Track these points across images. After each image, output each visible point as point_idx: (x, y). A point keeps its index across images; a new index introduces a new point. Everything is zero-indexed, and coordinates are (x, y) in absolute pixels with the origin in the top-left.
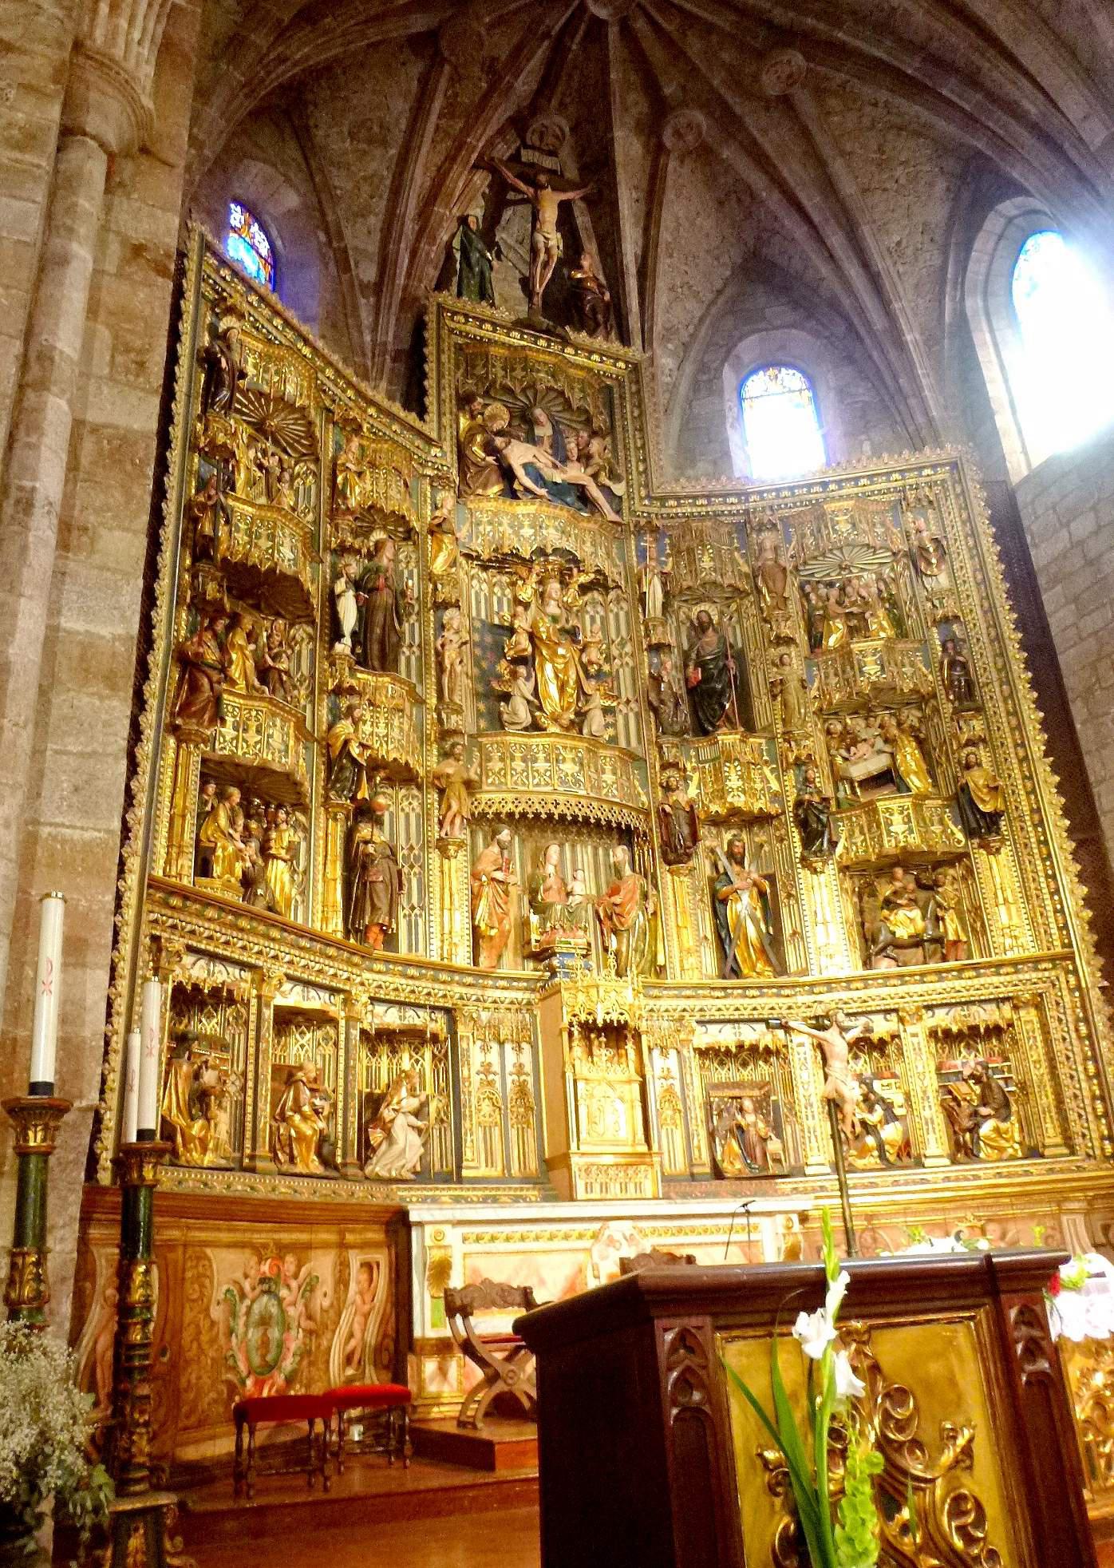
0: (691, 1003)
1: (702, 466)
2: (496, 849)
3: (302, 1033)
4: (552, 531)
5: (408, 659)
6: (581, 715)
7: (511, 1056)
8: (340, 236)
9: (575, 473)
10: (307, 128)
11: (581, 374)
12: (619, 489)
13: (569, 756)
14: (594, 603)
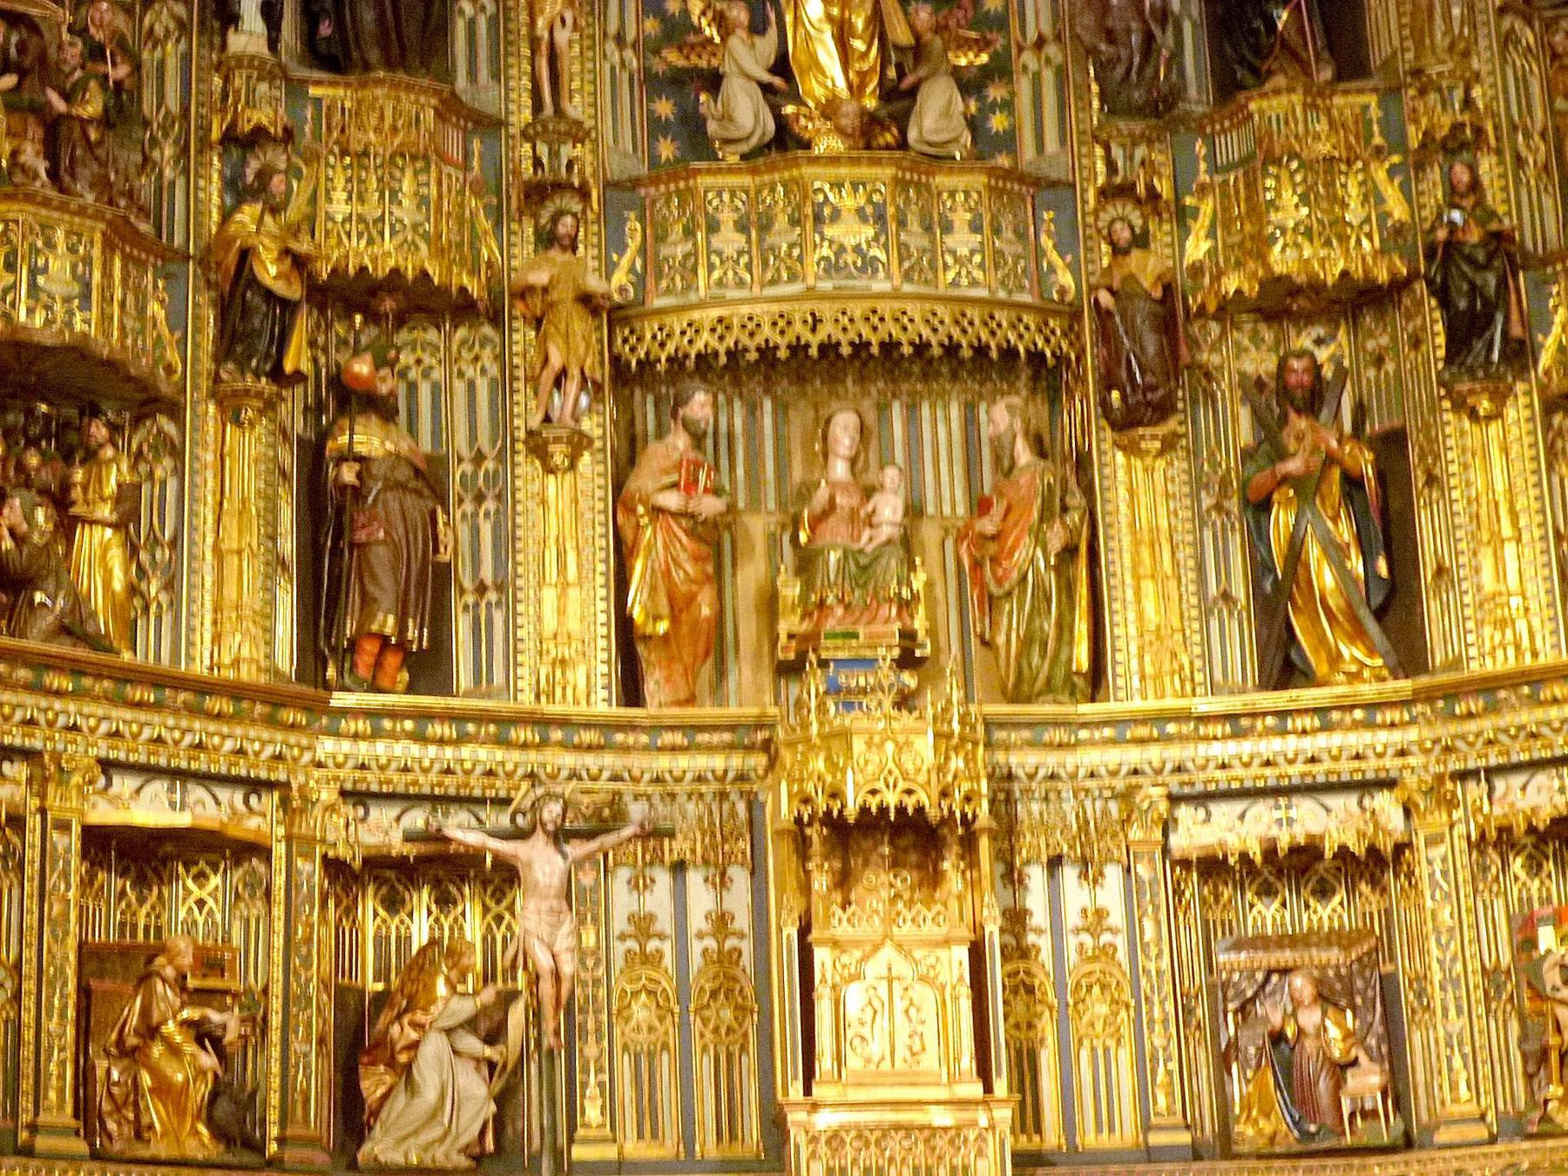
0: (1154, 753)
2: (679, 441)
3: (200, 877)
5: (472, 25)
6: (899, 98)
7: (701, 897)
13: (848, 201)
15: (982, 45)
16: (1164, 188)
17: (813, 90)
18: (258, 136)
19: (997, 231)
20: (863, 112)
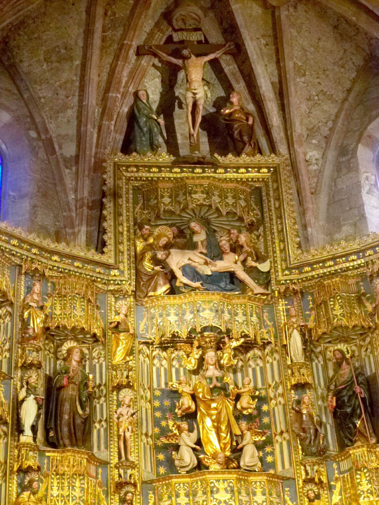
1: (347, 229)
4: (207, 312)
6: (237, 451)
8: (46, 131)
9: (229, 263)
10: (13, 65)
11: (231, 185)
12: (264, 267)
13: (222, 486)
14: (255, 357)
15: (264, 434)
16: (324, 479)
17: (209, 449)
18: (29, 470)
19: (271, 495)
20: (226, 457)
